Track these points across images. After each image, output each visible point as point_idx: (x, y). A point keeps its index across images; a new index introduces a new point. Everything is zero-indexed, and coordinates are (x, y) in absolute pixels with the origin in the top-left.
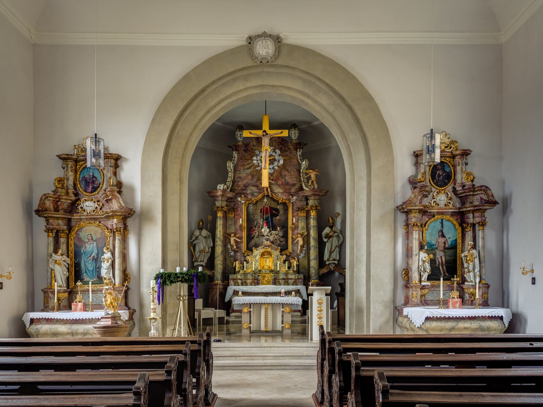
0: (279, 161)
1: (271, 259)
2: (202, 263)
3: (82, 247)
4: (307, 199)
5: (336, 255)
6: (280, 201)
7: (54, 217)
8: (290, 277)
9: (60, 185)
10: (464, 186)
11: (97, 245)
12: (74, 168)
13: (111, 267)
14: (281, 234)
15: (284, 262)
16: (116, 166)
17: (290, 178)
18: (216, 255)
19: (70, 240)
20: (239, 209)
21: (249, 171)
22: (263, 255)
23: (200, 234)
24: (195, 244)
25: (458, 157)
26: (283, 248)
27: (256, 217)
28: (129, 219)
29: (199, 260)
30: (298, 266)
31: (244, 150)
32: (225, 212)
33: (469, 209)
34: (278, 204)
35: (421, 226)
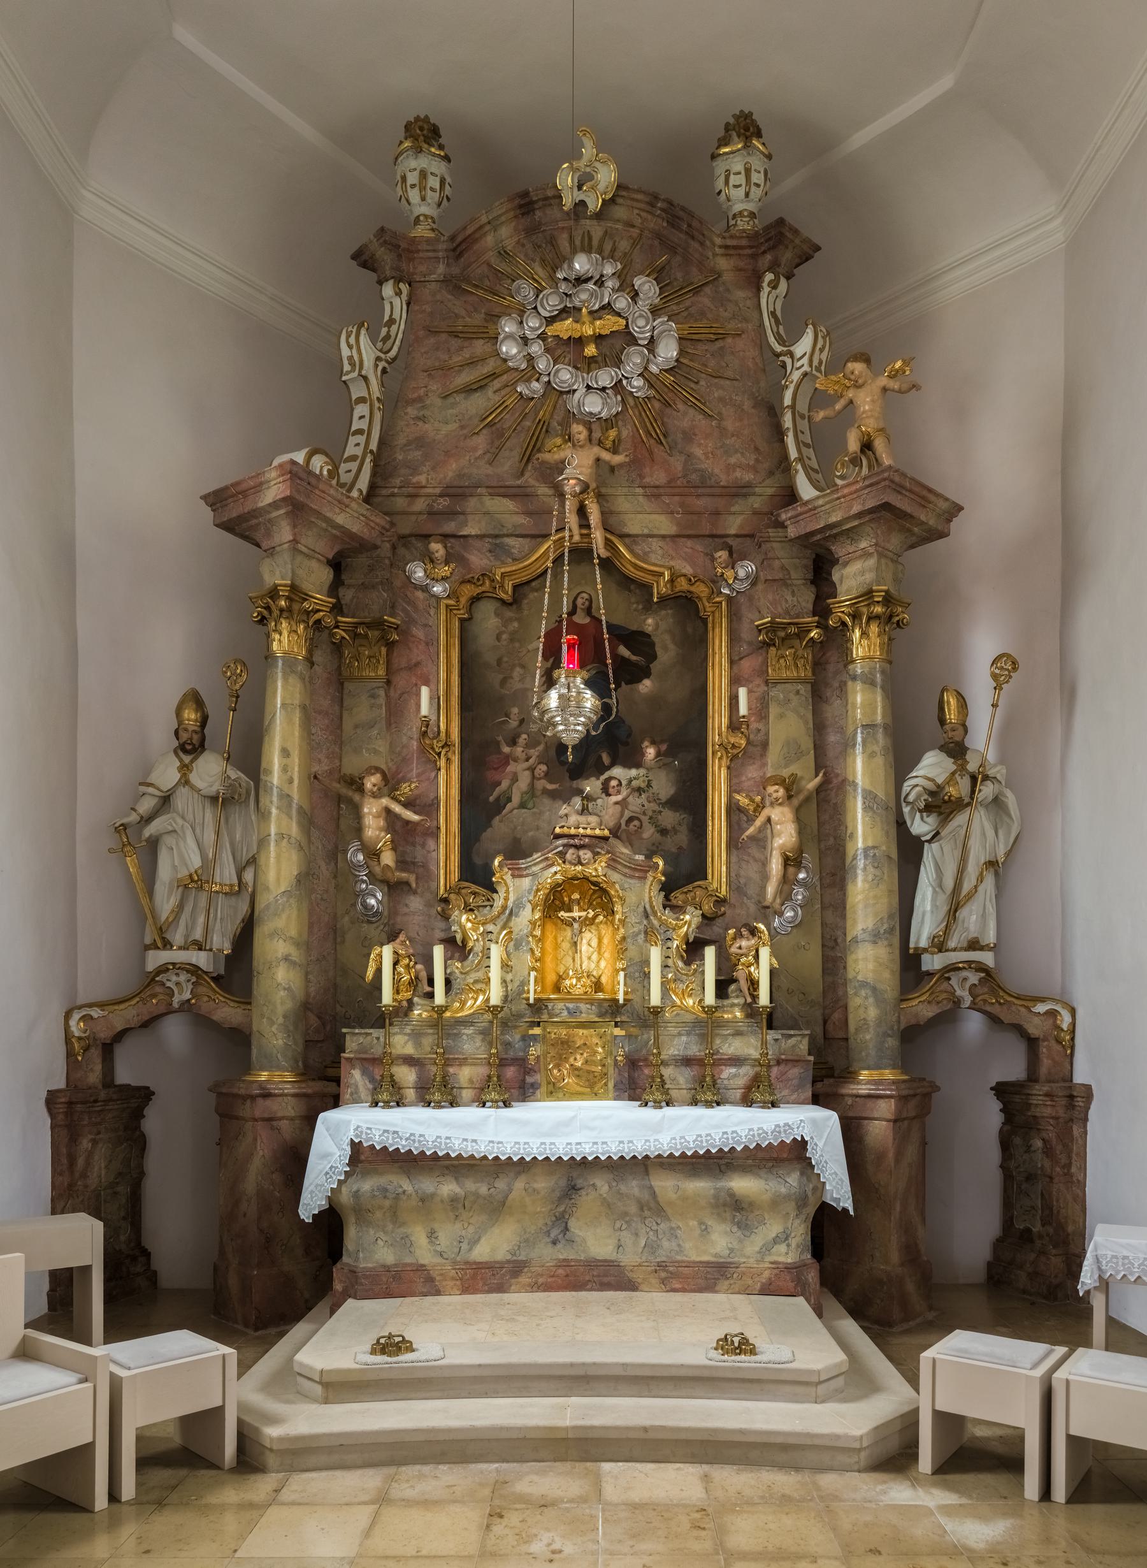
0: (652, 343)
1: (607, 932)
5: (984, 916)
6: (661, 588)
8: (732, 1047)
14: (664, 786)
15: (693, 949)
17: (719, 450)
20: (418, 632)
21: (478, 403)
22: (554, 903)
23: (185, 781)
26: (684, 875)
27: (515, 685)
29: (178, 938)
31: (446, 281)
34: (649, 607)
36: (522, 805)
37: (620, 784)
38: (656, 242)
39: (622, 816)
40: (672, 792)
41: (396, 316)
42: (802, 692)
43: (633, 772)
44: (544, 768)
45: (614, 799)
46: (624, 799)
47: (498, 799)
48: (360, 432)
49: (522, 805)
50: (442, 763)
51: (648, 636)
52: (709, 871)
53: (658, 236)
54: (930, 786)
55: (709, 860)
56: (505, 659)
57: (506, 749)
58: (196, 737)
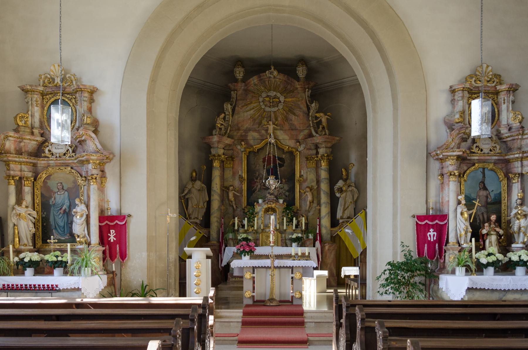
2: (196, 220)
3: (51, 197)
4: (317, 147)
6: (286, 150)
7: (16, 162)
9: (23, 122)
10: (510, 129)
11: (69, 196)
12: (39, 102)
13: (85, 223)
16: (92, 101)
18: (212, 211)
19: (35, 189)
23: (193, 187)
24: (187, 199)
25: (503, 93)
28: (107, 165)
30: (306, 224)
32: (223, 162)
33: (517, 156)
35: (459, 175)
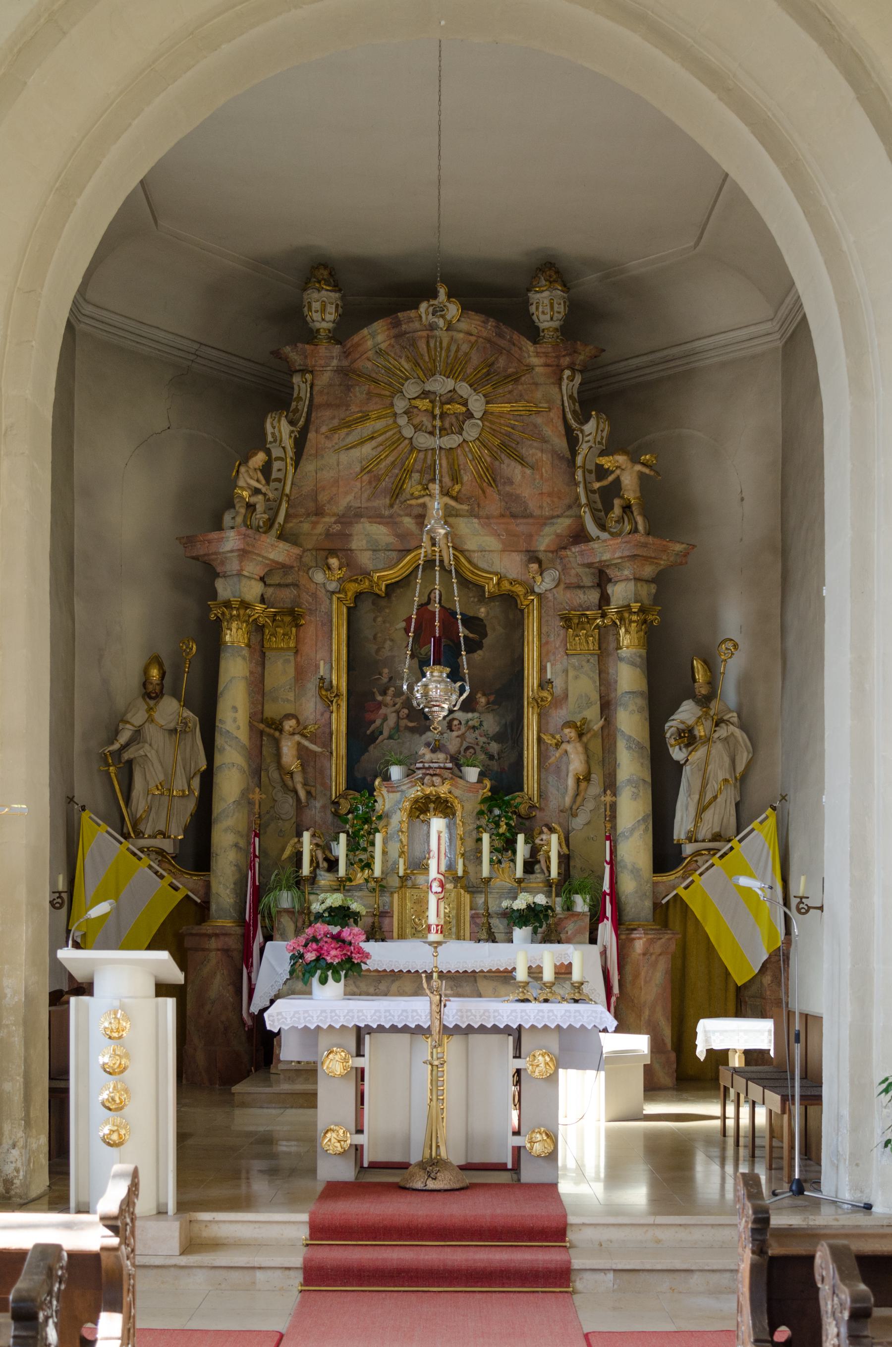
23: (150, 719)
29: (148, 832)
36: (390, 737)
37: (460, 723)
38: (488, 345)
39: (461, 745)
40: (497, 729)
41: (302, 395)
42: (591, 661)
43: (470, 715)
44: (406, 711)
45: (455, 734)
46: (463, 734)
47: (373, 732)
48: (278, 480)
49: (390, 737)
50: (334, 707)
51: (482, 620)
52: (525, 786)
53: (489, 341)
54: (681, 726)
55: (525, 778)
56: (379, 635)
57: (379, 698)
58: (158, 688)
